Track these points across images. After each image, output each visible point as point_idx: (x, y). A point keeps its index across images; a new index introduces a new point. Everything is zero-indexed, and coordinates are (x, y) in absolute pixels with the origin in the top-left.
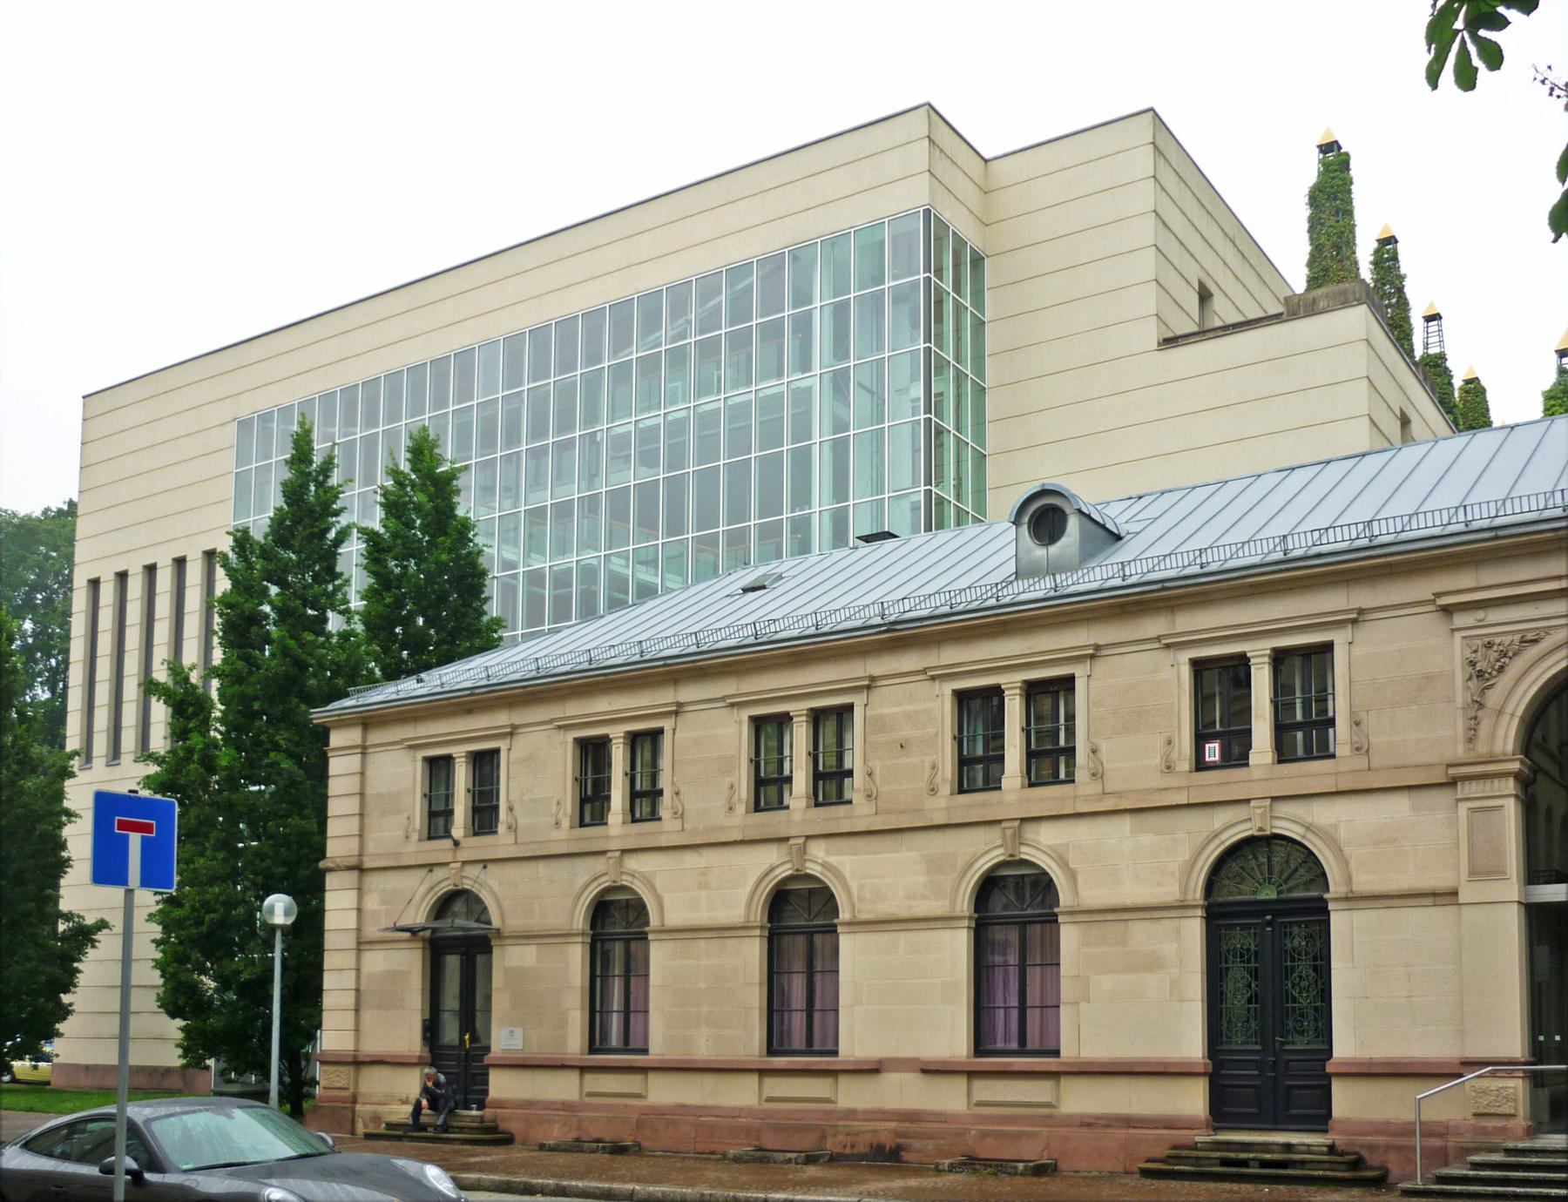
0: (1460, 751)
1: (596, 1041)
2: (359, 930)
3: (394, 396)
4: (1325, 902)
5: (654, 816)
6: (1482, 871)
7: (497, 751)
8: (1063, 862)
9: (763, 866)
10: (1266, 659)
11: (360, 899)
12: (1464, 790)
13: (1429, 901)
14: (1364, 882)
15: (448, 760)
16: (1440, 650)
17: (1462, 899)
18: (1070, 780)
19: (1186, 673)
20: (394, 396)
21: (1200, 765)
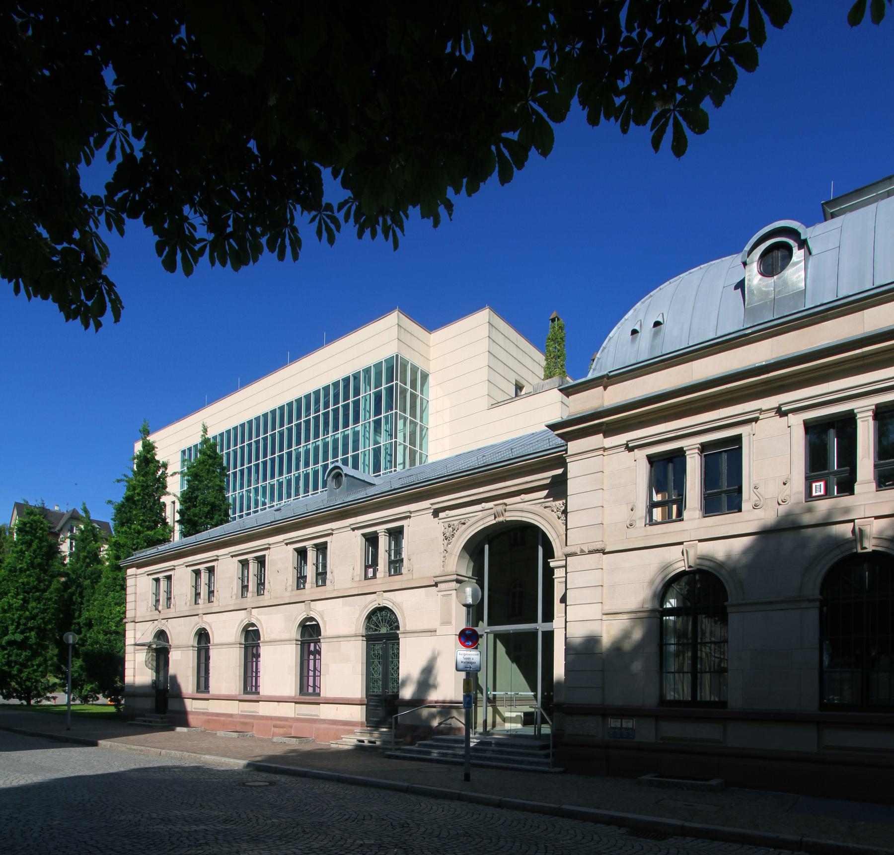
0: (438, 571)
1: (303, 687)
2: (566, 606)
3: (317, 401)
4: (398, 634)
5: (324, 584)
6: (446, 622)
7: (402, 527)
8: (322, 618)
9: (299, 613)
10: (871, 413)
11: (135, 634)
12: (441, 586)
13: (429, 634)
14: (408, 629)
15: (679, 456)
16: (436, 527)
17: (438, 633)
18: (304, 588)
19: (799, 433)
20: (317, 401)
21: (366, 578)
